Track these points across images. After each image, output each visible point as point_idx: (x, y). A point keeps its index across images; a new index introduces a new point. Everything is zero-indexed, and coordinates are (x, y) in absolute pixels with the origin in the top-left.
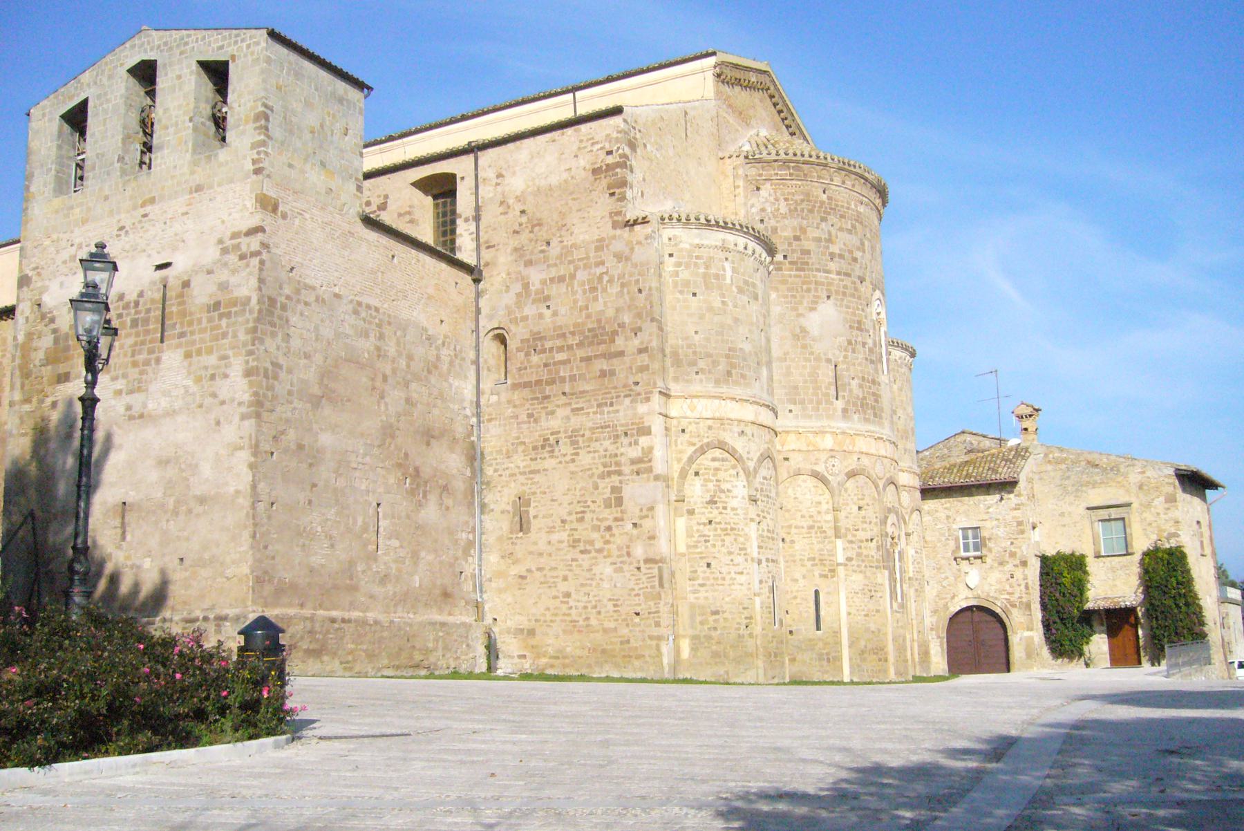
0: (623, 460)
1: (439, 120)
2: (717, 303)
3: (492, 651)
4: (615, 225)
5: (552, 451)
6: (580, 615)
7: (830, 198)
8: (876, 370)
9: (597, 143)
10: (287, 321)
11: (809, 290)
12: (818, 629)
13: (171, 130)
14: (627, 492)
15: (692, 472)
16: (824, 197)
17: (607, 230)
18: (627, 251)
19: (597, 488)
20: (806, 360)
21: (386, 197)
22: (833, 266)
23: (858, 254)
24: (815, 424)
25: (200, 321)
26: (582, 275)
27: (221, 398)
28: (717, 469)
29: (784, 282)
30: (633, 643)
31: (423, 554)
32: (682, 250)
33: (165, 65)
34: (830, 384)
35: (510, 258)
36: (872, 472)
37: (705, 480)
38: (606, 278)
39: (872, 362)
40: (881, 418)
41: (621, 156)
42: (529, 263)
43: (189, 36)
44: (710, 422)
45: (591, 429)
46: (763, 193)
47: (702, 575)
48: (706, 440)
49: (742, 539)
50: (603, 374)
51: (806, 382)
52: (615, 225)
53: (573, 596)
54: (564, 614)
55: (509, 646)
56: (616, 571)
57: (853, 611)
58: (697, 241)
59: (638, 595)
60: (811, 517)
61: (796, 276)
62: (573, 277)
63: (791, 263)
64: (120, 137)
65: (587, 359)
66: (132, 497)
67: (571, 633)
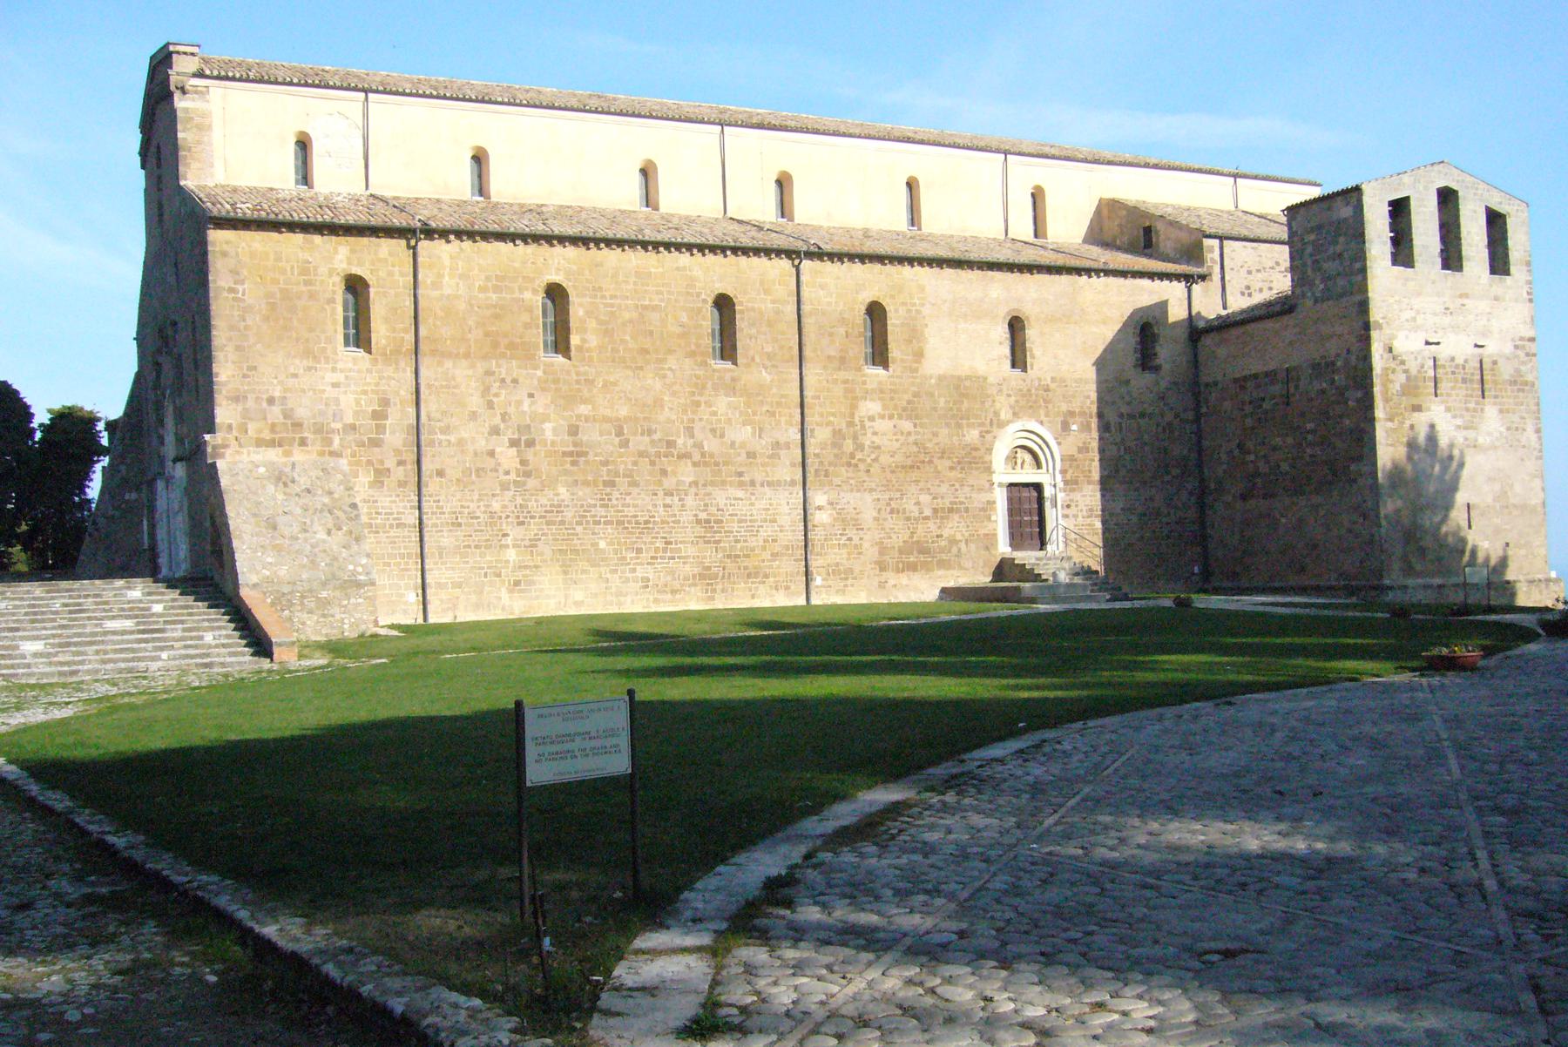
1: (1255, 172)
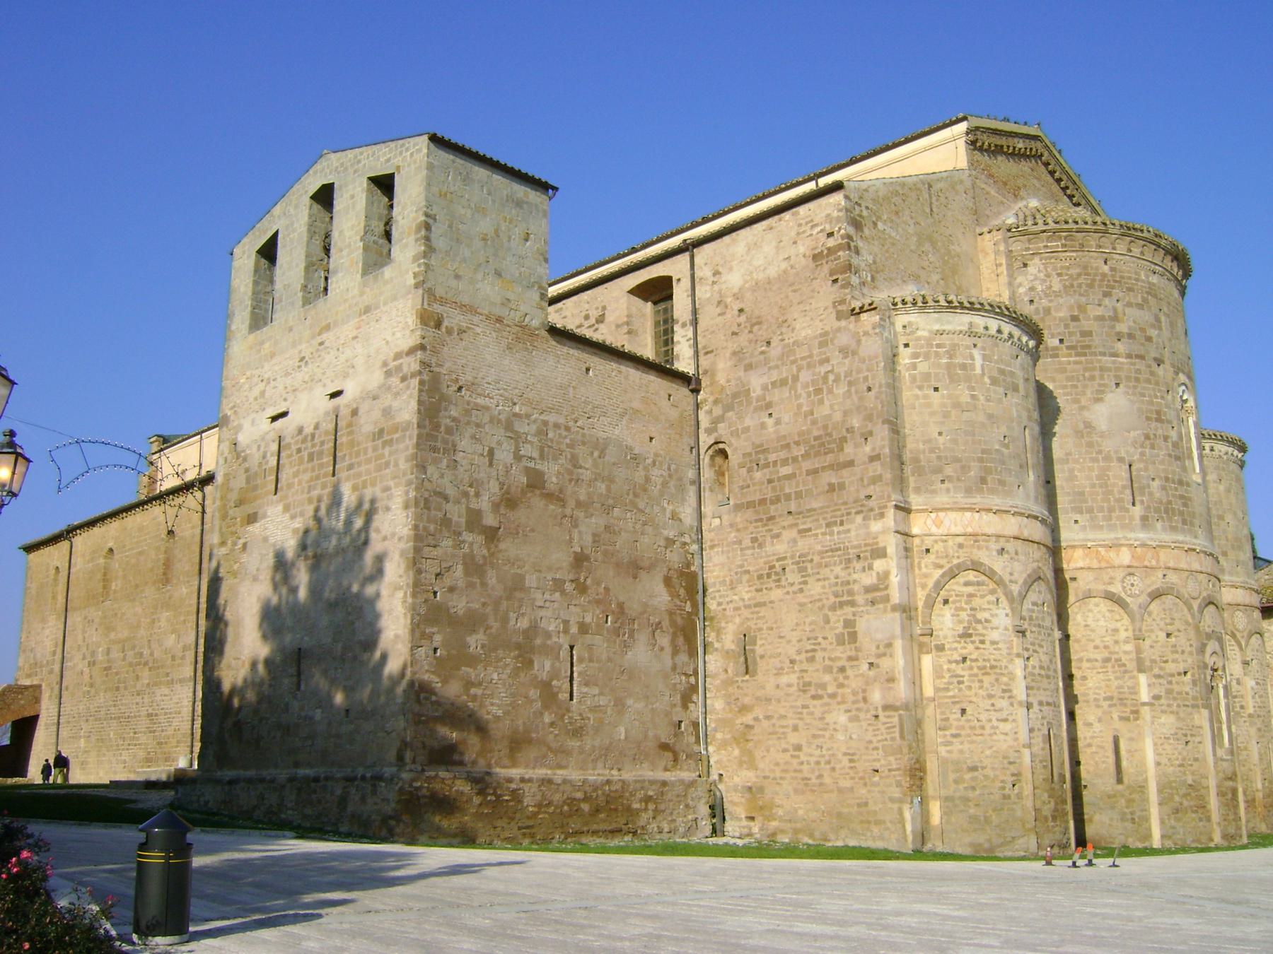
0: (856, 587)
2: (965, 398)
3: (717, 811)
4: (840, 316)
5: (779, 580)
6: (813, 771)
7: (1112, 269)
8: (1184, 469)
9: (816, 225)
10: (454, 446)
11: (1092, 378)
12: (1120, 780)
13: (345, 252)
14: (861, 626)
15: (940, 599)
16: (1106, 268)
17: (831, 322)
18: (854, 345)
19: (828, 622)
20: (1094, 460)
21: (604, 308)
22: (1121, 347)
23: (1153, 333)
24: (1107, 536)
25: (366, 450)
26: (805, 376)
27: (384, 533)
28: (971, 596)
29: (1063, 370)
30: (872, 807)
31: (630, 702)
32: (919, 339)
33: (341, 187)
34: (1124, 487)
35: (729, 364)
36: (1183, 591)
37: (957, 609)
38: (831, 377)
39: (1178, 458)
40: (1192, 524)
41: (842, 237)
42: (749, 367)
43: (361, 153)
44: (960, 540)
45: (821, 553)
46: (1031, 269)
47: (955, 723)
48: (955, 561)
49: (1005, 679)
50: (832, 488)
51: (1093, 486)
52: (840, 316)
53: (805, 749)
54: (795, 771)
55: (736, 807)
56: (851, 720)
57: (1164, 761)
58: (937, 327)
59: (876, 748)
60: (1106, 647)
61: (1076, 363)
62: (796, 378)
63: (1068, 348)
64: (303, 265)
65: (814, 472)
66: (307, 642)
67: (803, 793)
